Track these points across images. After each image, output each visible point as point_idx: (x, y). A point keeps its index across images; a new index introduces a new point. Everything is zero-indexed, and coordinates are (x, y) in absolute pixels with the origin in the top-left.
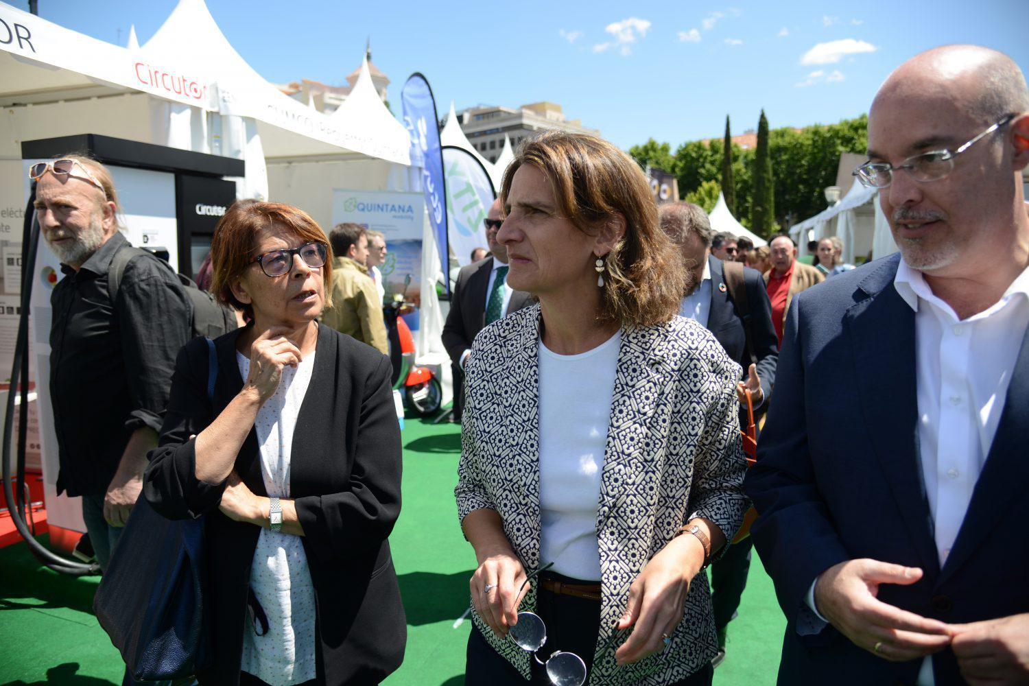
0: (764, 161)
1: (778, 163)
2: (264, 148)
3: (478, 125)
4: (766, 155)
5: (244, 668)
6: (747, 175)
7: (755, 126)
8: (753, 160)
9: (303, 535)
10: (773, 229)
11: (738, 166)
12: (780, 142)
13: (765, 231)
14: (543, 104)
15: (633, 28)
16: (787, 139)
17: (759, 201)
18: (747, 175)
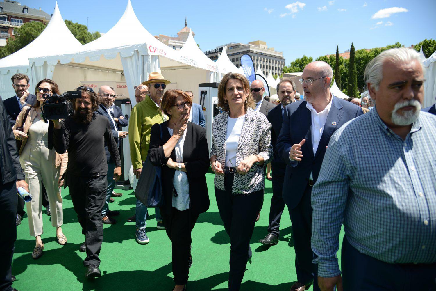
0: (353, 65)
1: (360, 65)
2: (63, 18)
3: (231, 51)
4: (354, 62)
5: (173, 206)
6: (346, 70)
7: (349, 49)
8: (348, 64)
9: (186, 172)
10: (357, 93)
11: (343, 66)
12: (361, 56)
13: (353, 94)
14: (258, 41)
15: (298, 6)
16: (363, 54)
17: (351, 81)
18: (346, 70)
